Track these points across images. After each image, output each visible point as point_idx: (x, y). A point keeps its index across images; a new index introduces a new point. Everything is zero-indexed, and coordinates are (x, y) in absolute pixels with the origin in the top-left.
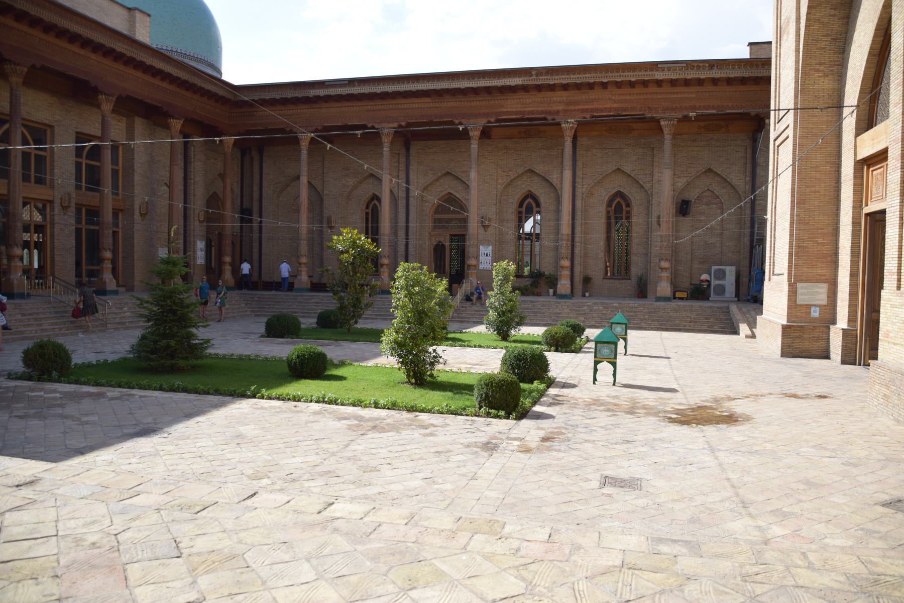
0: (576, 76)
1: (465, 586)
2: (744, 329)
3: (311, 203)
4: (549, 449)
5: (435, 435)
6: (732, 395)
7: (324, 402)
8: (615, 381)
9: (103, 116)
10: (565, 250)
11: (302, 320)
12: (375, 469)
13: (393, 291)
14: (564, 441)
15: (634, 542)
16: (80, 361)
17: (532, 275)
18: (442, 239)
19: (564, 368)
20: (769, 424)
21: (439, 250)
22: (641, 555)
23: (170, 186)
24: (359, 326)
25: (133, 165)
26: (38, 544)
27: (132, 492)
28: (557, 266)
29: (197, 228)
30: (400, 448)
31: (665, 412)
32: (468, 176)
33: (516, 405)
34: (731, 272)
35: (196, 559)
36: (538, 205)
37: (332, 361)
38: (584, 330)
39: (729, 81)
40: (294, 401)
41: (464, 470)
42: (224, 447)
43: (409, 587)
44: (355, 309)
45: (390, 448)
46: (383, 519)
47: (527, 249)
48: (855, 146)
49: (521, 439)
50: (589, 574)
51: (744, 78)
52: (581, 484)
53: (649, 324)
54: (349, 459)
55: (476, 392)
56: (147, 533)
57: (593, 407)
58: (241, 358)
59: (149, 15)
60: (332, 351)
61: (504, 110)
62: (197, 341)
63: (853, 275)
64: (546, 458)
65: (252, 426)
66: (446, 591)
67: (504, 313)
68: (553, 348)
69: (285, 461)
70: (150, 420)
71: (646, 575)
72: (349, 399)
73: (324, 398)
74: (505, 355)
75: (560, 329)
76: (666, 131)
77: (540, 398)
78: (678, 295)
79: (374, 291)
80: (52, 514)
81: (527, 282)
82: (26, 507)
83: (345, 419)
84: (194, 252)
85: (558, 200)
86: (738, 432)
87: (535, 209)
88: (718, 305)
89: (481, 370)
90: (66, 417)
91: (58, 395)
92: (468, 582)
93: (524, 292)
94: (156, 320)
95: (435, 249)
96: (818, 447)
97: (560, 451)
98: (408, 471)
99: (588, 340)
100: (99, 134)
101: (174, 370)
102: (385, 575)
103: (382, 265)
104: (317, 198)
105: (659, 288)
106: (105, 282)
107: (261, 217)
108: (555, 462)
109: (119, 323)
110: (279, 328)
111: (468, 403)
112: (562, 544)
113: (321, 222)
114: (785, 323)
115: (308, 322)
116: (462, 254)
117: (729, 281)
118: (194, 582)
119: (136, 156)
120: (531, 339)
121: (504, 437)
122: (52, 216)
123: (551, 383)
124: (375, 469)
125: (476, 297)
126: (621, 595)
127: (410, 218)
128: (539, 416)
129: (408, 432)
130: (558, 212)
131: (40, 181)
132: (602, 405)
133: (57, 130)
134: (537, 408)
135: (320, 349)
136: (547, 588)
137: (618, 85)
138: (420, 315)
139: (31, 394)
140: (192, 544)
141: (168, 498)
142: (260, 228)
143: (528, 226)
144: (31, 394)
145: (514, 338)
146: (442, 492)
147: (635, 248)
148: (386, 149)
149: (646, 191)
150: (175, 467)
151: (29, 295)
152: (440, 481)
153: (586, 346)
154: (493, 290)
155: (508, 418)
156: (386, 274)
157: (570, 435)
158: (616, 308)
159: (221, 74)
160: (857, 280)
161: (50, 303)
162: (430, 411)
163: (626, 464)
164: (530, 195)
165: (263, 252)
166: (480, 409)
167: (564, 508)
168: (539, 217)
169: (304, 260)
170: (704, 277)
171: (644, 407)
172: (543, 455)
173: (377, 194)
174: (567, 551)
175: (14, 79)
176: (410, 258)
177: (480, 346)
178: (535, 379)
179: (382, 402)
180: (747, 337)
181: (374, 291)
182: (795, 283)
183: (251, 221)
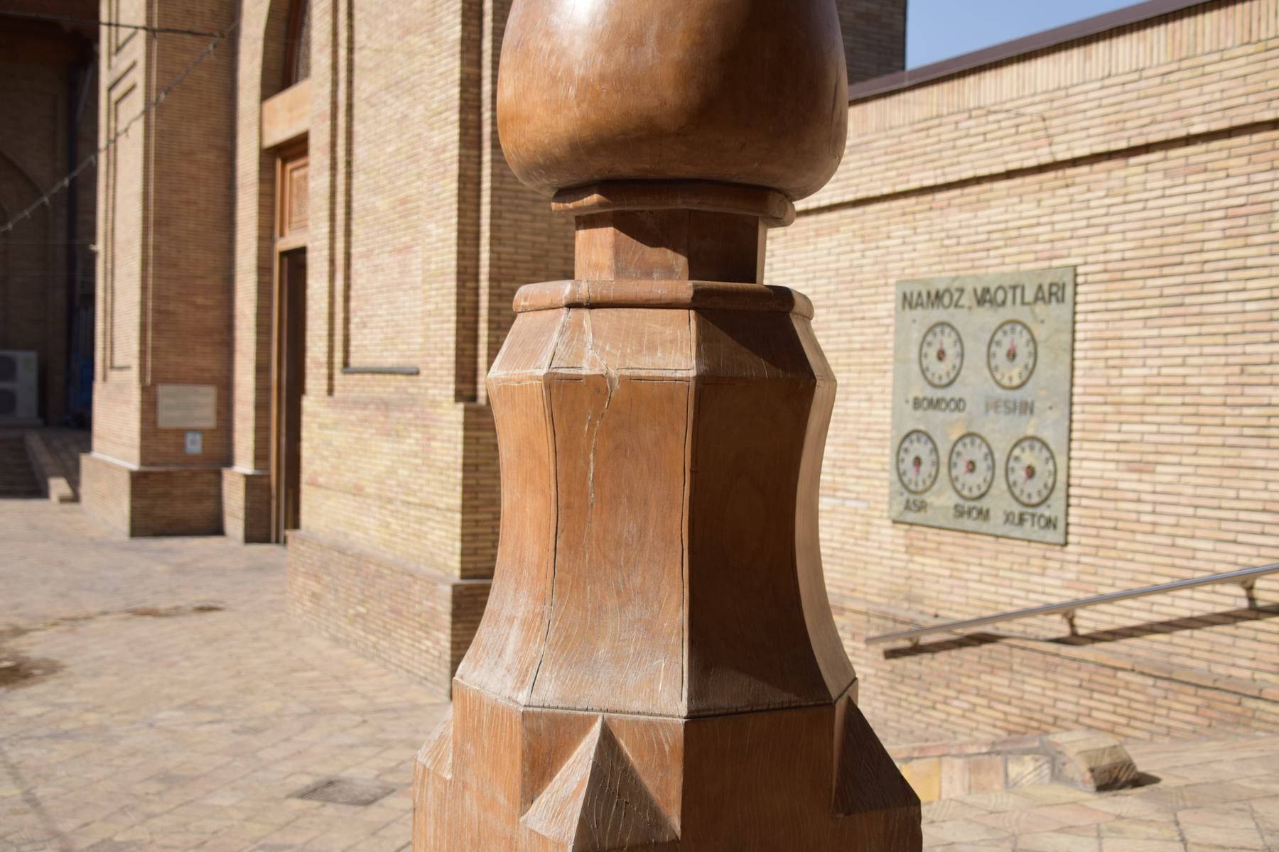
2: (58, 486)
20: (96, 674)
48: (261, 121)
63: (262, 369)
86: (29, 698)
96: (193, 706)
114: (135, 466)
160: (268, 378)
180: (63, 500)
182: (154, 384)
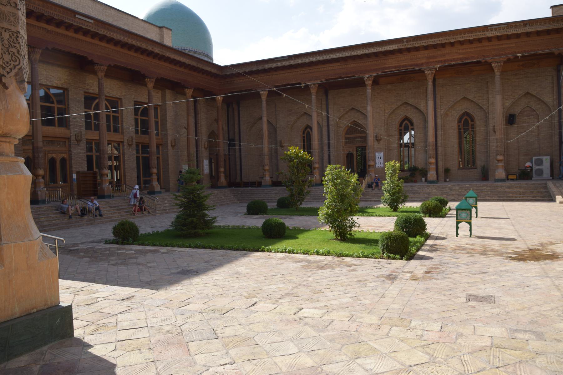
0: (433, 40)
1: (391, 357)
3: (269, 133)
4: (431, 278)
5: (356, 271)
6: (553, 241)
7: (286, 252)
8: (471, 234)
9: (148, 91)
10: (432, 152)
11: (268, 204)
12: (320, 292)
13: (324, 183)
14: (440, 273)
15: (497, 331)
16: (143, 233)
17: (410, 169)
18: (351, 150)
19: (436, 227)
21: (349, 157)
22: (504, 339)
23: (187, 128)
24: (302, 206)
25: (166, 118)
26: (137, 331)
27: (185, 303)
28: (427, 163)
29: (204, 153)
30: (335, 279)
31: (507, 253)
32: (366, 109)
33: (407, 251)
34: (546, 160)
35: (227, 340)
36: (412, 124)
37: (288, 227)
38: (447, 203)
39: (538, 33)
40: (268, 252)
41: (376, 292)
42: (229, 279)
43: (356, 357)
44: (300, 195)
45: (329, 279)
46: (334, 318)
47: (406, 153)
49: (412, 272)
50: (470, 351)
51: (538, 31)
52: (454, 300)
53: (492, 197)
54: (304, 286)
55: (380, 243)
56: (197, 325)
57: (457, 251)
58: (234, 228)
59: (171, 30)
60: (291, 222)
61: (387, 66)
62: (209, 218)
64: (430, 284)
65: (244, 267)
66: (379, 360)
67: (394, 194)
68: (427, 215)
69: (266, 288)
70: (185, 264)
71: (509, 352)
72: (300, 250)
73: (285, 250)
74: (397, 220)
75: (431, 202)
76: (496, 70)
77: (421, 247)
78: (510, 177)
79: (311, 184)
80: (143, 315)
81: (407, 174)
82: (129, 311)
83: (299, 262)
84: (203, 166)
85: (425, 121)
86: (559, 265)
87: (410, 127)
88: (539, 182)
89: (382, 230)
90: (139, 264)
91: (133, 252)
92: (392, 355)
93: (406, 180)
94: (185, 206)
95: (347, 157)
97: (438, 279)
98: (341, 293)
99: (450, 209)
100: (147, 101)
101: (196, 236)
102: (340, 350)
103: (314, 168)
104: (273, 130)
105: (497, 173)
106: (154, 187)
107: (240, 142)
108: (435, 286)
109: (163, 210)
110: (254, 209)
111: (375, 251)
112: (450, 333)
113: (276, 144)
115: (272, 205)
116: (364, 159)
117: (546, 166)
118: (227, 353)
119: (168, 113)
120: (412, 210)
121: (400, 271)
122: (123, 150)
123: (428, 237)
124: (320, 292)
125: (375, 185)
126: (493, 363)
127: (331, 138)
128: (422, 258)
129: (338, 269)
130: (425, 128)
131: (116, 130)
132: (463, 250)
133: (123, 101)
134: (420, 253)
135: (281, 220)
136: (444, 359)
137: (461, 43)
138: (342, 197)
139: (118, 251)
140: (223, 331)
141: (205, 306)
142: (240, 149)
143: (406, 138)
144: (118, 251)
145: (401, 210)
146: (363, 305)
147: (479, 148)
148: (314, 97)
149: (484, 110)
150: (202, 291)
151: (113, 196)
152: (362, 298)
153: (449, 213)
154: (386, 180)
155: (401, 259)
156: (318, 174)
157: (444, 269)
158: (468, 187)
159: (212, 60)
161: (124, 200)
162: (351, 256)
163: (483, 287)
164: (406, 119)
165: (243, 164)
166: (383, 254)
167: (444, 315)
168: (413, 132)
169: (267, 168)
170: (528, 164)
171: (492, 250)
172: (426, 282)
173: (309, 124)
174: (454, 337)
175: (101, 74)
176: (331, 162)
177: (380, 216)
178: (418, 235)
179: (321, 251)
181: (311, 184)
183: (234, 145)
